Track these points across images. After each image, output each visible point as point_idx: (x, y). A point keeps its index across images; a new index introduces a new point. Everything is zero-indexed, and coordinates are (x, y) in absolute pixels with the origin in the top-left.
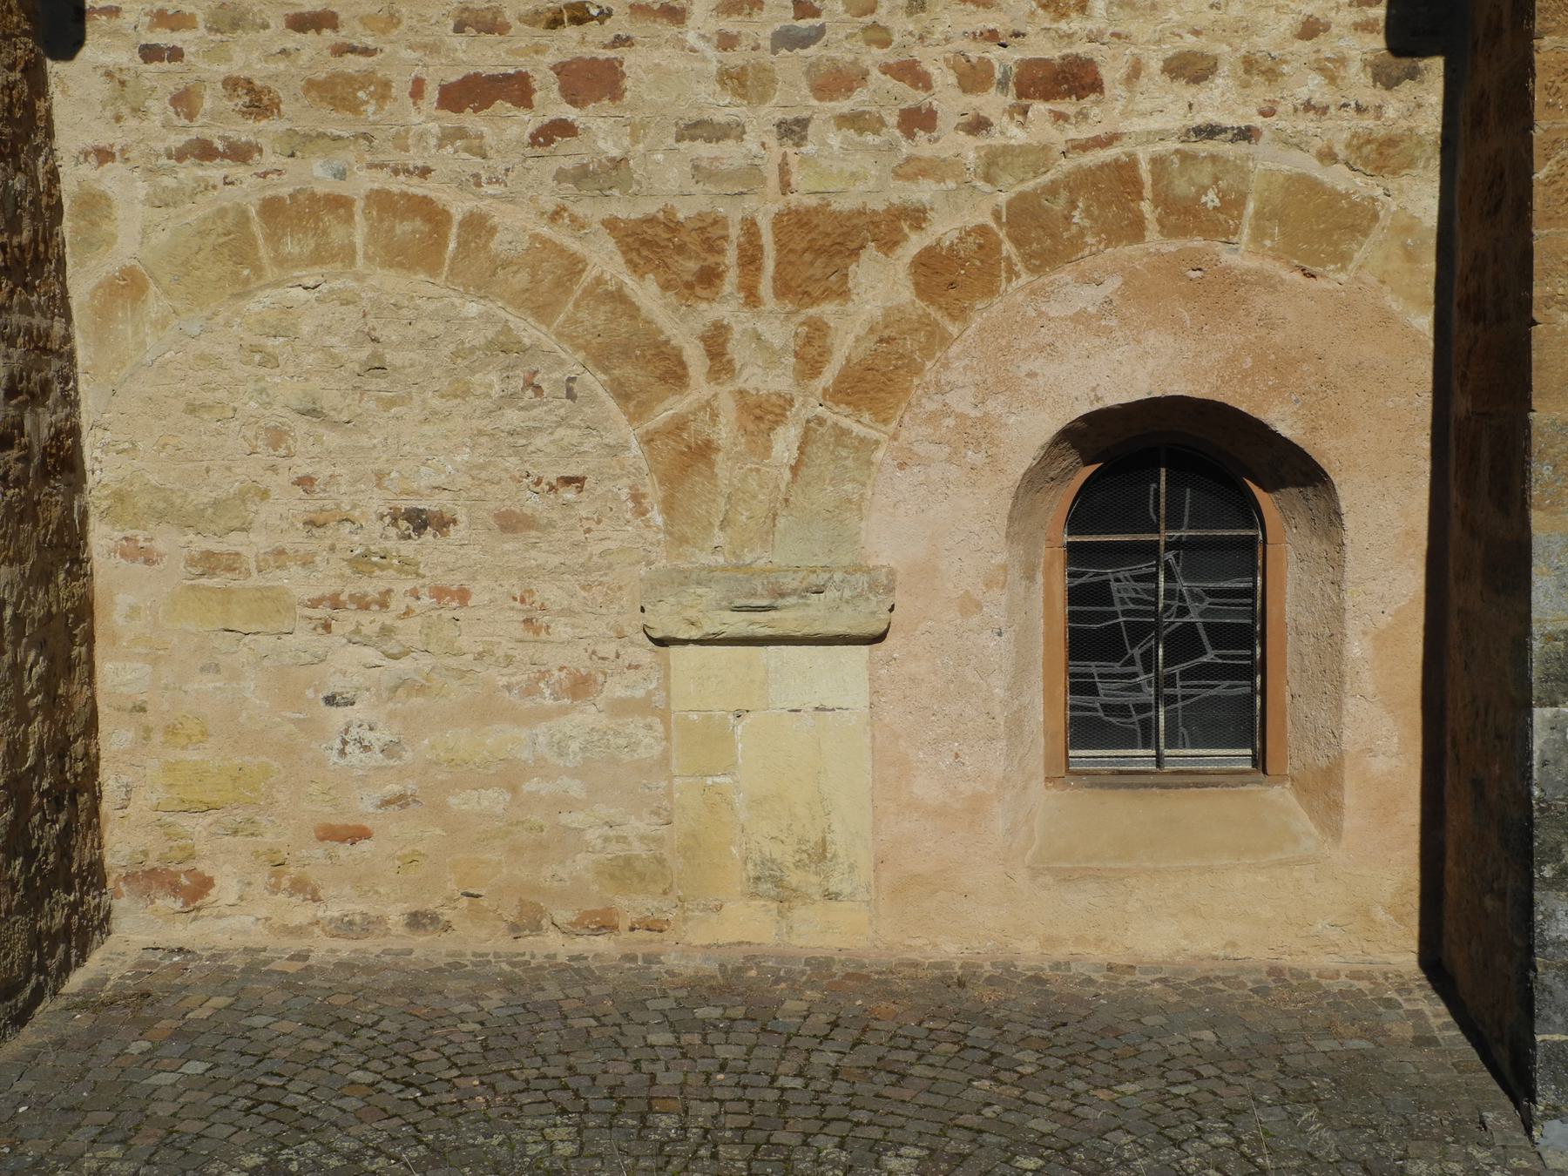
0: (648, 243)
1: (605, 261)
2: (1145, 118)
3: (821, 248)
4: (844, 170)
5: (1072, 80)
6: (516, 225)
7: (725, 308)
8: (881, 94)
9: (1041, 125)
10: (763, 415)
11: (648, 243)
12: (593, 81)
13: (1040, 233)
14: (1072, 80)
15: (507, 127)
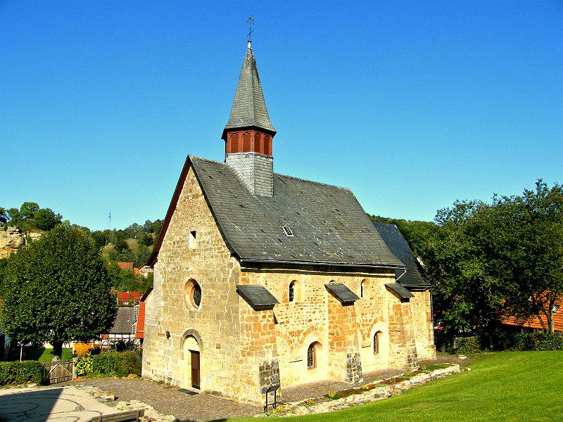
0: (290, 333)
1: (288, 335)
2: (313, 323)
3: (299, 332)
4: (300, 328)
5: (311, 320)
6: (284, 333)
7: (294, 337)
8: (302, 322)
9: (309, 324)
10: (296, 345)
11: (290, 333)
12: (288, 322)
13: (309, 331)
14: (311, 320)
15: (283, 325)
